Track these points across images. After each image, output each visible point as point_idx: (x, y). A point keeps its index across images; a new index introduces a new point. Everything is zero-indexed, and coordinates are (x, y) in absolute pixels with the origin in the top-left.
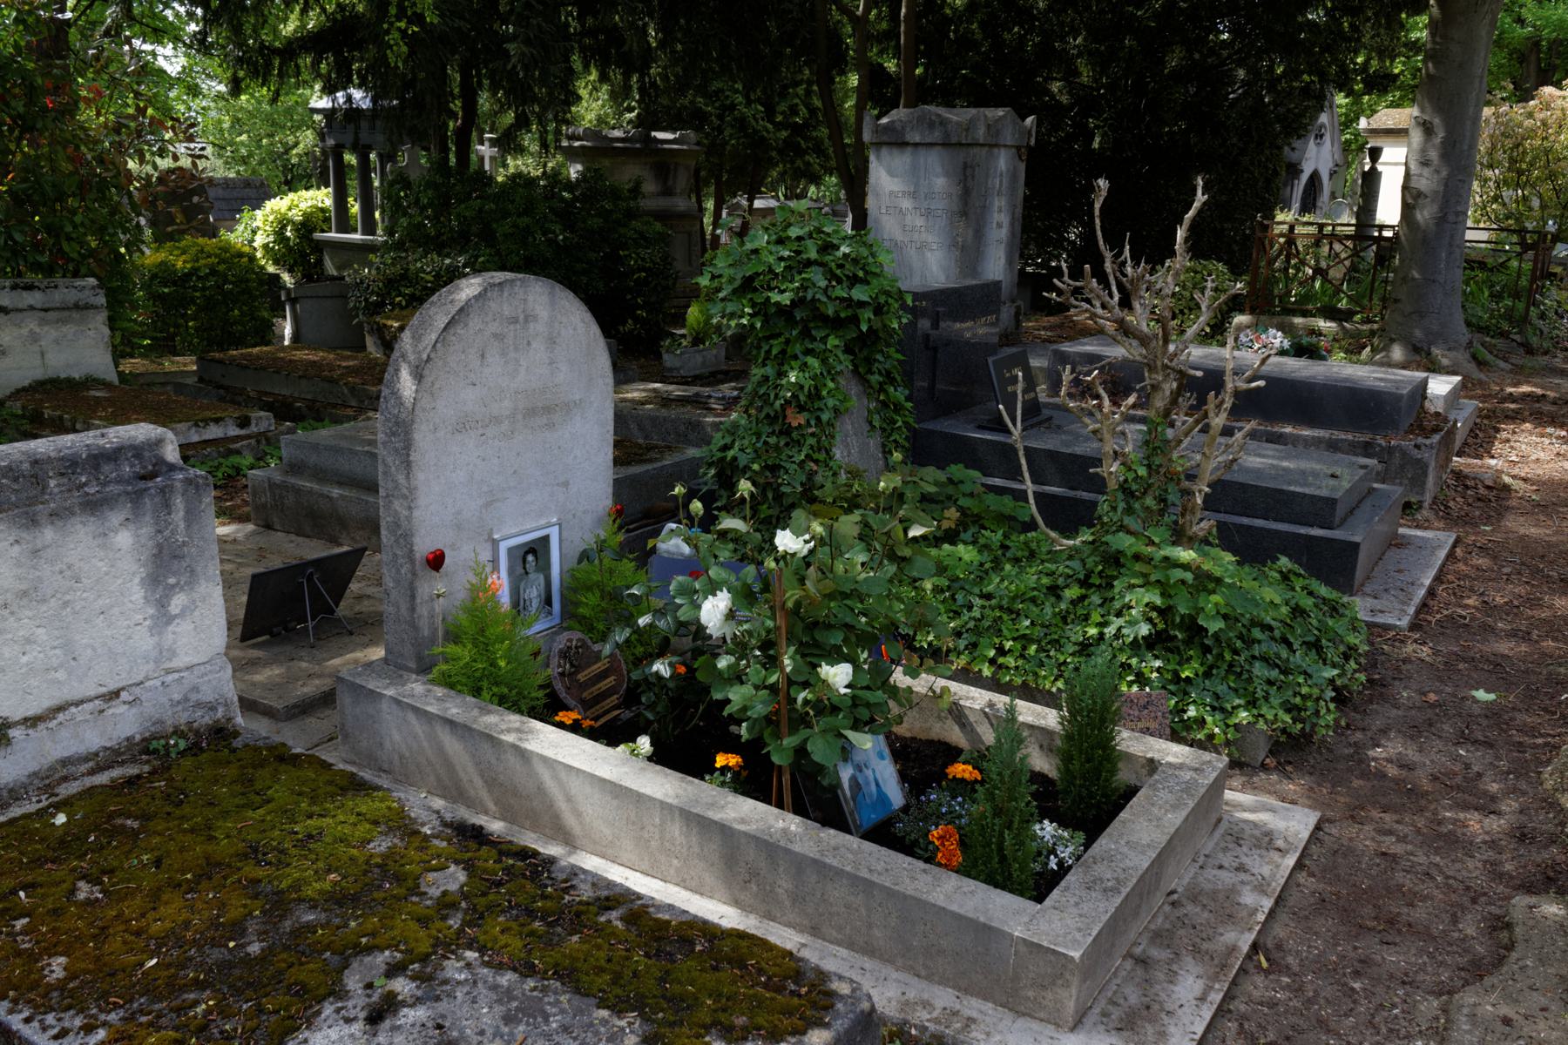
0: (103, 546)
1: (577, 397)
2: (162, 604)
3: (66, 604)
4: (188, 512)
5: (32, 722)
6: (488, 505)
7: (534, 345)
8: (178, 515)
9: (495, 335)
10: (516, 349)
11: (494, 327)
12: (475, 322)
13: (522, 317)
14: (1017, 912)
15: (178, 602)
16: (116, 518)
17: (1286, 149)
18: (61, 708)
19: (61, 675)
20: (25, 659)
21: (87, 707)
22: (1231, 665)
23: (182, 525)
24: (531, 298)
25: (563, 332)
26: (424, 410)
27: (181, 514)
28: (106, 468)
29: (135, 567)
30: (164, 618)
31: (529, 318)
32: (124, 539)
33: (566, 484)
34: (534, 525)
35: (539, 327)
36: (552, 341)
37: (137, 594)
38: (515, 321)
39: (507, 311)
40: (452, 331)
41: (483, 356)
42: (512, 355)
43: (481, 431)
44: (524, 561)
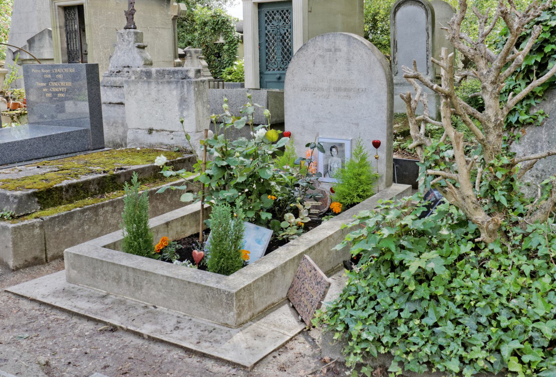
4: (187, 90)
5: (157, 131)
6: (317, 122)
7: (339, 61)
8: (185, 90)
9: (320, 56)
10: (330, 62)
11: (320, 52)
13: (333, 49)
18: (162, 130)
21: (167, 132)
22: (342, 364)
24: (337, 42)
26: (289, 80)
28: (176, 75)
33: (357, 124)
34: (339, 138)
36: (349, 61)
37: (177, 108)
38: (330, 50)
39: (326, 46)
40: (301, 52)
41: (314, 63)
43: (313, 92)
44: (331, 150)
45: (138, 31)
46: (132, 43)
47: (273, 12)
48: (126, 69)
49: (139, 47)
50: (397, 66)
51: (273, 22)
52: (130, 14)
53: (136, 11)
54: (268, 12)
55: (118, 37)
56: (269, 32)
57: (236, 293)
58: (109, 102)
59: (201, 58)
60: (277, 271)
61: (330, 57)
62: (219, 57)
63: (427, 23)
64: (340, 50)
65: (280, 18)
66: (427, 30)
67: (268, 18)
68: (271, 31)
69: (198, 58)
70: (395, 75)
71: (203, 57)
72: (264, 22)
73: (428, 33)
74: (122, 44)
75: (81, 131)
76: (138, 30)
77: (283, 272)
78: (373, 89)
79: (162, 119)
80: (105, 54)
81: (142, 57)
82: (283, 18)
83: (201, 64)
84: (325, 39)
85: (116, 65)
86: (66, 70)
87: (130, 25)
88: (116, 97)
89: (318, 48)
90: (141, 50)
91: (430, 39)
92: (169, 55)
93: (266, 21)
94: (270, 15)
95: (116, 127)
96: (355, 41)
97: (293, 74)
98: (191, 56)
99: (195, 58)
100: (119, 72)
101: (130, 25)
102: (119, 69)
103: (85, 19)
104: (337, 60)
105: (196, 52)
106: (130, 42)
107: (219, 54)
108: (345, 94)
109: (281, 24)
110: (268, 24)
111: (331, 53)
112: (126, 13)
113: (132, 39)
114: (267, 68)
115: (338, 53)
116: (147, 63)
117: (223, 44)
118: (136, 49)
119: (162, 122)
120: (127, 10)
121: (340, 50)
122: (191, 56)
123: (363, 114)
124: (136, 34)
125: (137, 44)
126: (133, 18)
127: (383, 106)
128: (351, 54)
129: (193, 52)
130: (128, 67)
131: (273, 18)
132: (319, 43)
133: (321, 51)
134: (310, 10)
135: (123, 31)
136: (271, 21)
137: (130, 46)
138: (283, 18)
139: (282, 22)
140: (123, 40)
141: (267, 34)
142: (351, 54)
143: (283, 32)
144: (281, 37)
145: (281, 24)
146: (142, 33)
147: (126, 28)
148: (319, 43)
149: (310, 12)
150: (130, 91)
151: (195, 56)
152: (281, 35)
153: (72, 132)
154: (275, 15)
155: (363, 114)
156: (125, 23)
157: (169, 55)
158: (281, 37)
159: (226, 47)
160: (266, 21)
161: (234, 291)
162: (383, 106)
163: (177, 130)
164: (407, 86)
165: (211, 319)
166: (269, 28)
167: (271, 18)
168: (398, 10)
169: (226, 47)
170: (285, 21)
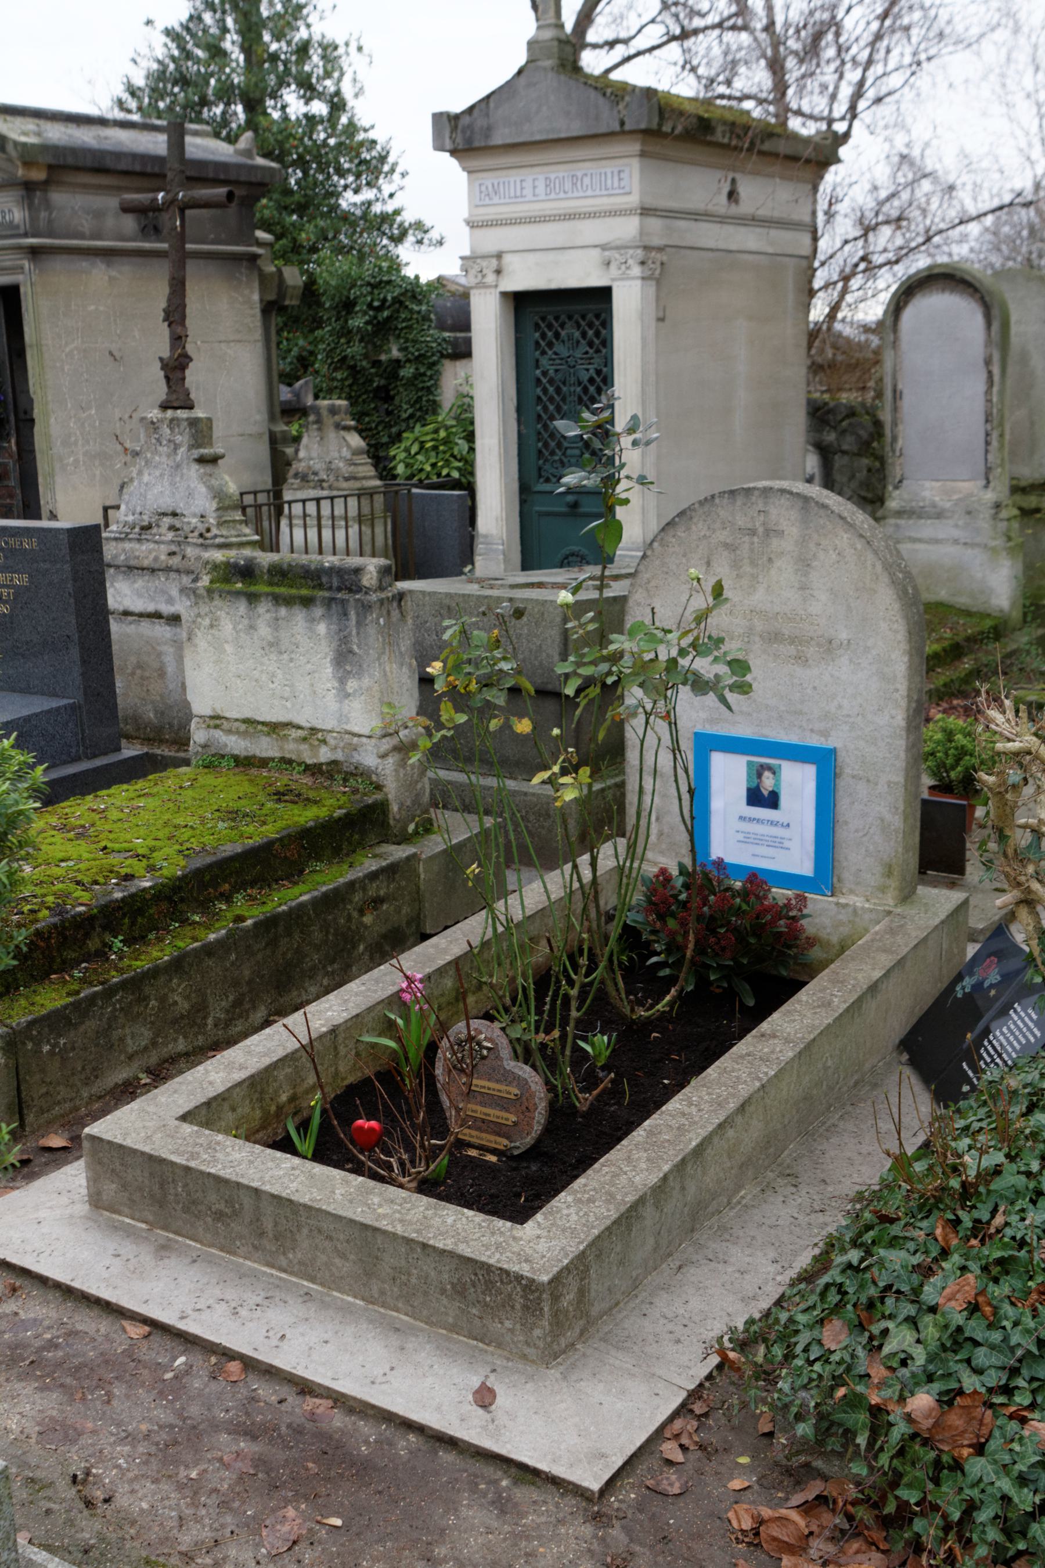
0: (310, 629)
1: (844, 635)
2: (342, 681)
3: (291, 660)
9: (726, 546)
10: (753, 563)
11: (723, 536)
12: (699, 528)
13: (761, 530)
14: (207, 1072)
15: (352, 685)
16: (318, 611)
17: (405, 252)
19: (289, 705)
20: (271, 686)
23: (354, 632)
24: (773, 511)
25: (821, 555)
26: (639, 604)
27: (354, 622)
29: (327, 650)
30: (344, 695)
31: (770, 532)
32: (322, 628)
35: (787, 544)
37: (328, 670)
38: (753, 532)
39: (741, 521)
40: (671, 532)
41: (708, 564)
42: (747, 569)
45: (201, 415)
46: (183, 450)
47: (557, 318)
48: (167, 521)
49: (201, 460)
50: (901, 460)
51: (558, 347)
52: (175, 368)
53: (191, 360)
54: (543, 319)
55: (142, 431)
56: (545, 373)
57: (550, 1282)
58: (121, 609)
59: (347, 428)
60: (644, 1204)
61: (752, 550)
62: (389, 399)
63: (988, 342)
64: (780, 533)
65: (577, 334)
66: (988, 362)
67: (543, 336)
68: (551, 372)
69: (339, 427)
70: (896, 487)
71: (353, 423)
72: (531, 346)
73: (990, 373)
74: (156, 452)
75: (58, 709)
76: (199, 413)
77: (657, 1206)
78: (869, 643)
79: (286, 695)
80: (83, 424)
81: (210, 488)
82: (584, 335)
83: (348, 446)
84: (739, 503)
85: (139, 509)
86: (12, 541)
87: (178, 398)
88: (140, 595)
89: (718, 525)
90: (209, 468)
91: (995, 389)
92: (258, 417)
93: (537, 343)
94: (550, 326)
95: (142, 678)
96: (822, 512)
97: (648, 590)
98: (318, 421)
99: (332, 428)
100: (149, 527)
101: (178, 398)
102: (146, 519)
103: (26, 329)
104: (770, 560)
105: (333, 411)
106: (177, 447)
107: (388, 391)
108: (792, 650)
109: (578, 354)
110: (543, 353)
111: (756, 539)
112: (165, 366)
113: (183, 438)
114: (540, 476)
115: (775, 542)
116: (227, 503)
117: (397, 364)
118: (195, 466)
119: (289, 705)
120: (166, 354)
121: (780, 533)
122: (318, 421)
123: (840, 707)
124: (194, 422)
125: (196, 453)
126: (184, 379)
127: (897, 690)
128: (812, 545)
129: (325, 413)
130: (174, 514)
131: (557, 335)
132: (722, 513)
133: (725, 533)
134: (661, 315)
135: (155, 414)
136: (550, 345)
137: (179, 458)
138: (584, 335)
139: (584, 347)
140: (158, 440)
141: (538, 380)
142: (812, 545)
143: (585, 377)
144: (579, 389)
145: (578, 354)
146: (209, 420)
147: (164, 407)
148: (722, 513)
149: (661, 319)
150: (199, 615)
151: (329, 421)
152: (580, 384)
153: (36, 715)
154: (562, 326)
155: (840, 707)
156: (161, 391)
157: (258, 417)
158: (579, 389)
159: (408, 371)
160: (537, 343)
161: (545, 1278)
162: (897, 690)
163: (329, 728)
164: (930, 518)
165: (482, 1341)
166: (544, 361)
167: (550, 334)
168: (906, 303)
169: (408, 371)
170: (591, 344)
